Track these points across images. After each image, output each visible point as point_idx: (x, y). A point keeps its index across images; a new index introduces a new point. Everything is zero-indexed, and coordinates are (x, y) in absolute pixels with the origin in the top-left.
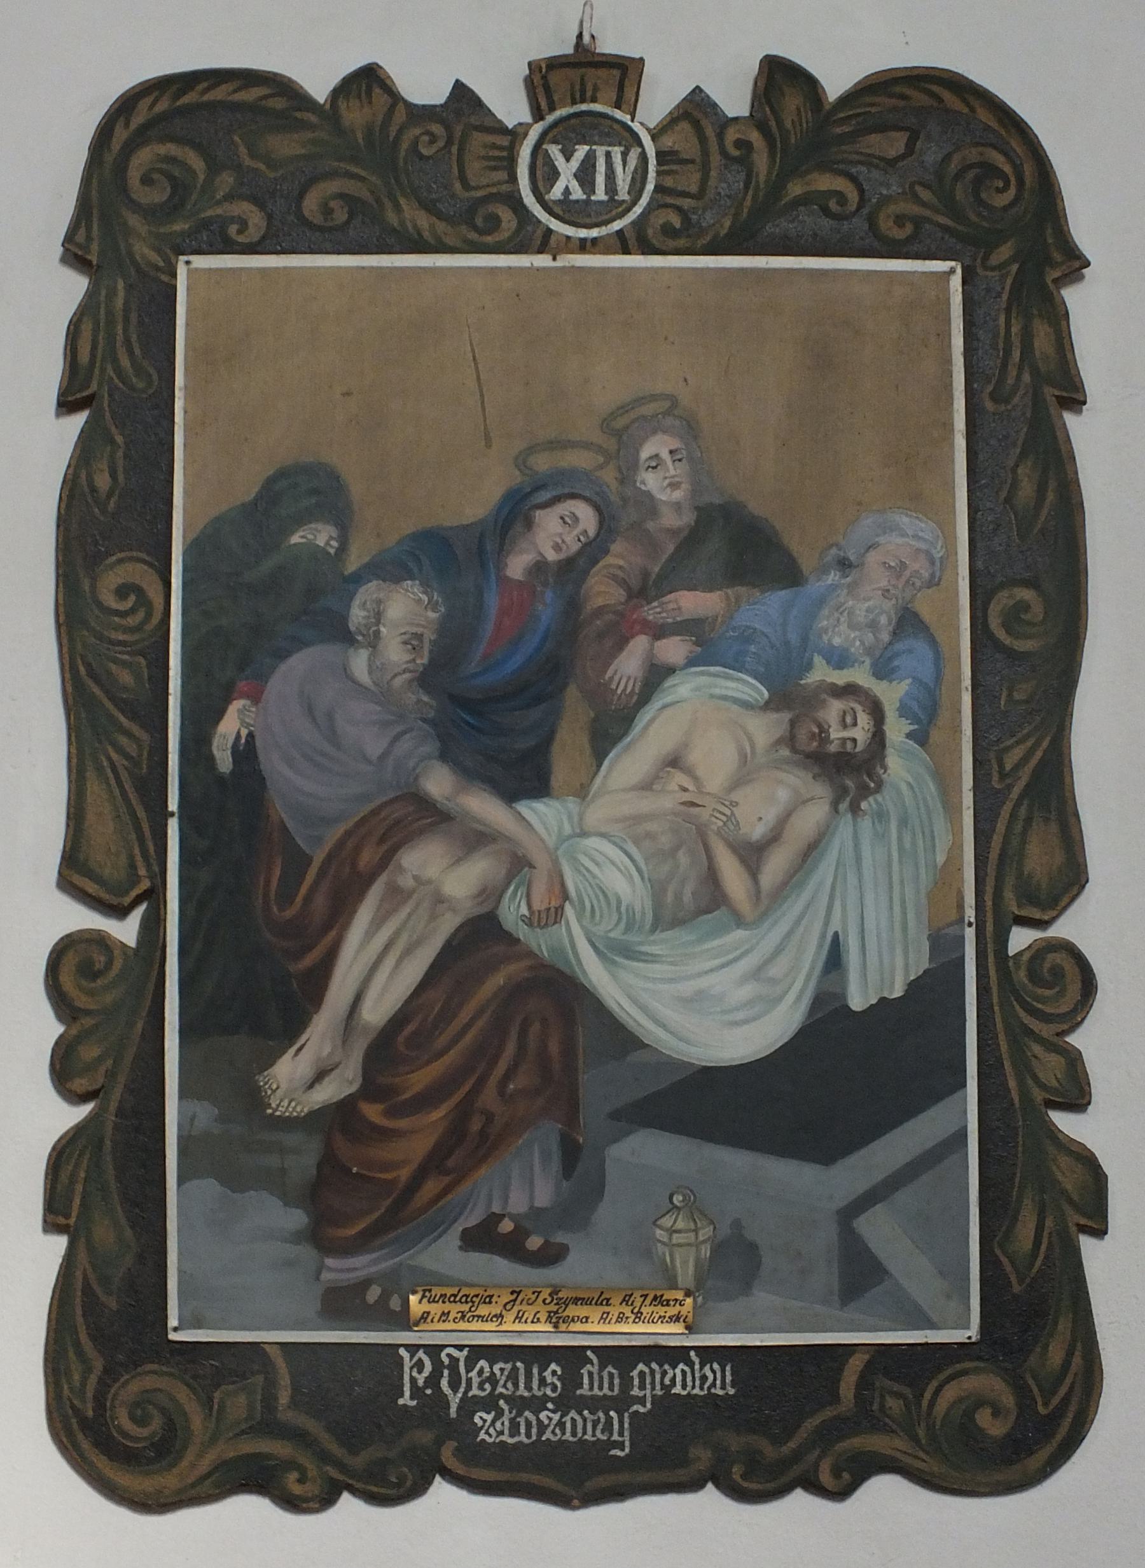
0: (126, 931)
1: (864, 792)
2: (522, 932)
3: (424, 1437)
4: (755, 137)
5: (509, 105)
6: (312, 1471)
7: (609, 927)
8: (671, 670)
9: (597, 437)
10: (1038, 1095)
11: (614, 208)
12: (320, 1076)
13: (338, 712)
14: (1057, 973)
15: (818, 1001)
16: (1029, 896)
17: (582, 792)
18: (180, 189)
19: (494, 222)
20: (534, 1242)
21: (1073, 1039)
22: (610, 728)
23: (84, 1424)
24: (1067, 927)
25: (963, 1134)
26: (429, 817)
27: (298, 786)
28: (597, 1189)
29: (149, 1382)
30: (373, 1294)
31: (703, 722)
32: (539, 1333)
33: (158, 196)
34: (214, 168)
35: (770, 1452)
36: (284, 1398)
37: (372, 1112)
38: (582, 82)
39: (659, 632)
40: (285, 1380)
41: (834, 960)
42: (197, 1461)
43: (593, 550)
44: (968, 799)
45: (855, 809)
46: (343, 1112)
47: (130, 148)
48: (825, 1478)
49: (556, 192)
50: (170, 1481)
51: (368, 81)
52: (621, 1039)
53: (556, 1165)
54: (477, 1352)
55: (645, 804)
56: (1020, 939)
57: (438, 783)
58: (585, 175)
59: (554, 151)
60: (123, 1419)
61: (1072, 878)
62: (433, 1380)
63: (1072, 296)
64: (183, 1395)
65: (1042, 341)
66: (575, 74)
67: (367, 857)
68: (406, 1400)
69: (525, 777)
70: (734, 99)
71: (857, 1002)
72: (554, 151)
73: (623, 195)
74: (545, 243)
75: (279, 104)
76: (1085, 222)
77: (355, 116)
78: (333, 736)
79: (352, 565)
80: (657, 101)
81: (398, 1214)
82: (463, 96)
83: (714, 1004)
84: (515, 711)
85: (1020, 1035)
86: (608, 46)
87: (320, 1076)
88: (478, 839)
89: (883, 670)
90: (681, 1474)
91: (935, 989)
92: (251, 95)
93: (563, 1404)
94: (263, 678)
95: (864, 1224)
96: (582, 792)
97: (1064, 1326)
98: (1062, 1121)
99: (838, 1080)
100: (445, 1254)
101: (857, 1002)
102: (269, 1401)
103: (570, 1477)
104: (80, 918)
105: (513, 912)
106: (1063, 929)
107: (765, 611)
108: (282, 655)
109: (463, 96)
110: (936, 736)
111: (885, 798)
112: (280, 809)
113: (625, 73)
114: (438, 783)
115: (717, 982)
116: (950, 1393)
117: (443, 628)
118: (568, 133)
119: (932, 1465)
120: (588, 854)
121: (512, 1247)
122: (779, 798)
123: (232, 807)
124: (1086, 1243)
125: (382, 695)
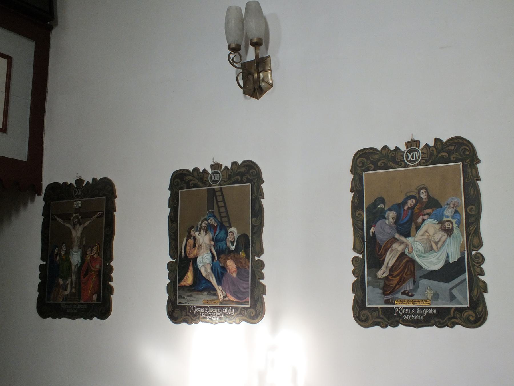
0: (361, 256)
1: (451, 234)
2: (408, 254)
3: (398, 319)
4: (434, 149)
5: (403, 148)
6: (384, 323)
7: (419, 253)
8: (425, 220)
9: (416, 191)
10: (477, 274)
11: (416, 160)
12: (384, 273)
13: (384, 229)
14: (479, 257)
15: (446, 262)
16: (474, 247)
17: (415, 236)
18: (363, 164)
19: (401, 164)
20: (410, 294)
21: (482, 266)
22: (418, 228)
23: (357, 317)
24: (262, 258)
25: (466, 279)
26: (396, 240)
27: (380, 237)
28: (418, 287)
29: (365, 312)
30: (391, 300)
31: (430, 226)
32: (412, 306)
33: (361, 165)
34: (367, 160)
35: (442, 321)
36: (380, 314)
37: (390, 277)
38: (412, 144)
39: (425, 215)
40: (380, 311)
41: (448, 256)
42: (370, 322)
43: (415, 205)
44: (465, 234)
45: (450, 237)
46: (387, 278)
47: (358, 158)
48: (449, 325)
49: (409, 159)
50: (367, 324)
51: (385, 147)
52: (420, 267)
53: (413, 283)
54: (404, 308)
55: (423, 237)
56: (474, 253)
57: (397, 236)
58: (412, 157)
59: (408, 154)
60: (362, 317)
61: (480, 245)
62: (398, 311)
63: (478, 165)
64: (368, 313)
65: (474, 172)
66: (411, 143)
67: (389, 245)
68: (395, 314)
69: (407, 235)
70: (432, 144)
71: (451, 262)
72: (408, 154)
73: (417, 159)
74: (408, 166)
75: (375, 151)
76: (480, 156)
77: (384, 152)
78: (384, 231)
79: (386, 209)
80: (422, 146)
81: (393, 291)
82: (397, 148)
83: (433, 263)
84: (406, 227)
85: (474, 265)
86: (416, 139)
87: (384, 273)
88: (402, 243)
89: (453, 218)
90: (430, 324)
91: (461, 260)
92: (371, 151)
93: (415, 314)
94: (376, 223)
95: (453, 291)
96: (415, 236)
97: (482, 305)
98: (481, 277)
99: (449, 272)
100: (399, 295)
101: (451, 262)
102: (379, 314)
103: (416, 324)
104: (357, 255)
105: (406, 252)
106: (480, 251)
107: (437, 211)
108: (378, 221)
109: (397, 148)
110: (460, 226)
111: (454, 235)
112: (378, 240)
113: (418, 143)
114: (397, 236)
115: (432, 260)
116: (466, 314)
117: (397, 215)
118: (410, 151)
119: (464, 324)
120: (415, 245)
121: (407, 294)
122: (440, 236)
123: (372, 240)
124: (485, 294)
125: (390, 225)
